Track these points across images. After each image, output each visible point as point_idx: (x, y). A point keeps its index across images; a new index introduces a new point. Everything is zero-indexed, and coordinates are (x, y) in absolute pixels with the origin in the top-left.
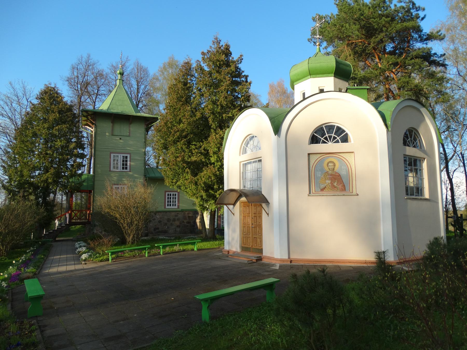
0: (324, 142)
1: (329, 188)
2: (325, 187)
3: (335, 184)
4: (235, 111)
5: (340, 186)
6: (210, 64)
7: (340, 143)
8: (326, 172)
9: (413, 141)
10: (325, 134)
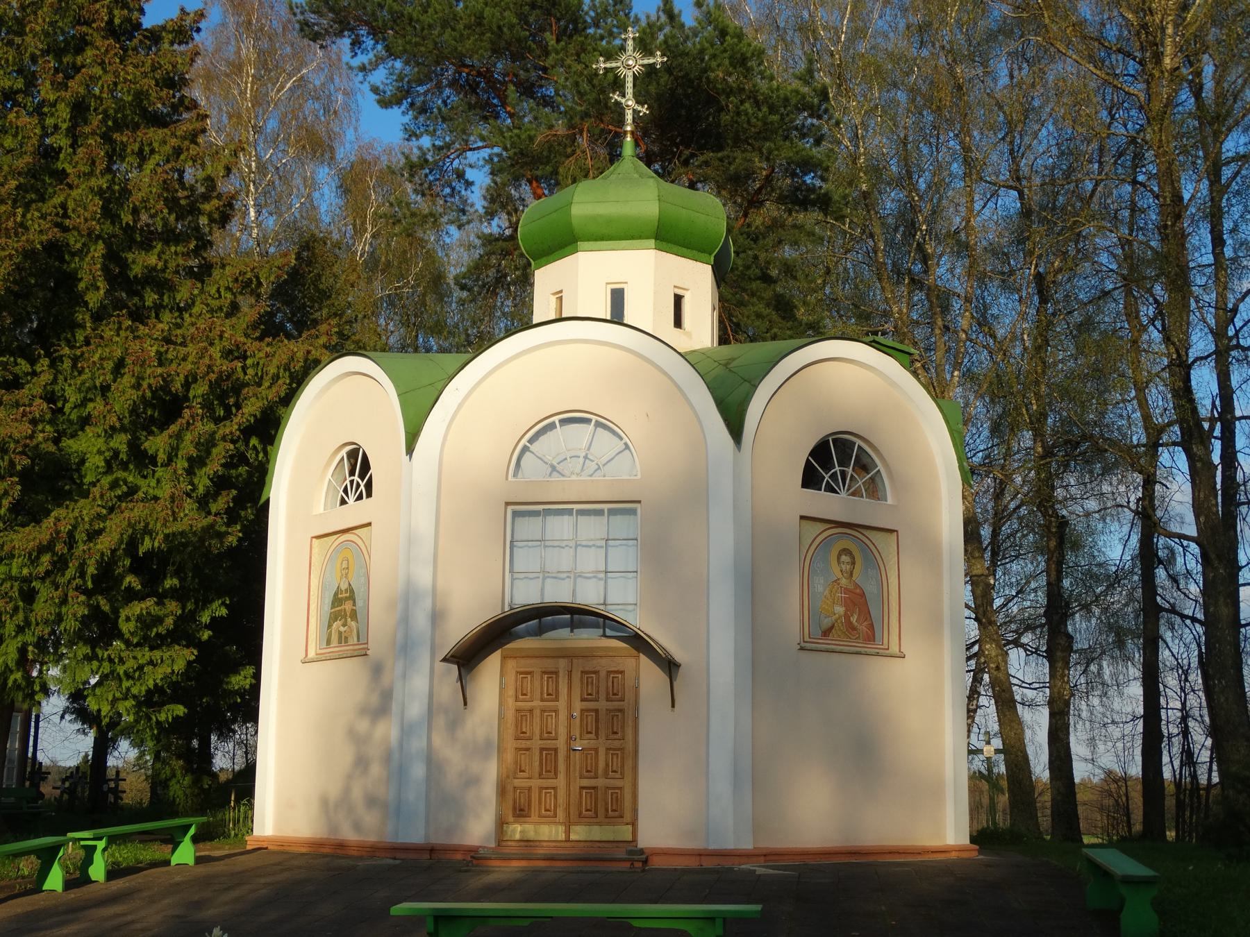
0: (830, 489)
1: (840, 630)
2: (832, 627)
3: (854, 619)
4: (176, 253)
5: (863, 628)
6: (543, 128)
7: (865, 499)
8: (835, 581)
9: (361, 491)
10: (848, 466)
